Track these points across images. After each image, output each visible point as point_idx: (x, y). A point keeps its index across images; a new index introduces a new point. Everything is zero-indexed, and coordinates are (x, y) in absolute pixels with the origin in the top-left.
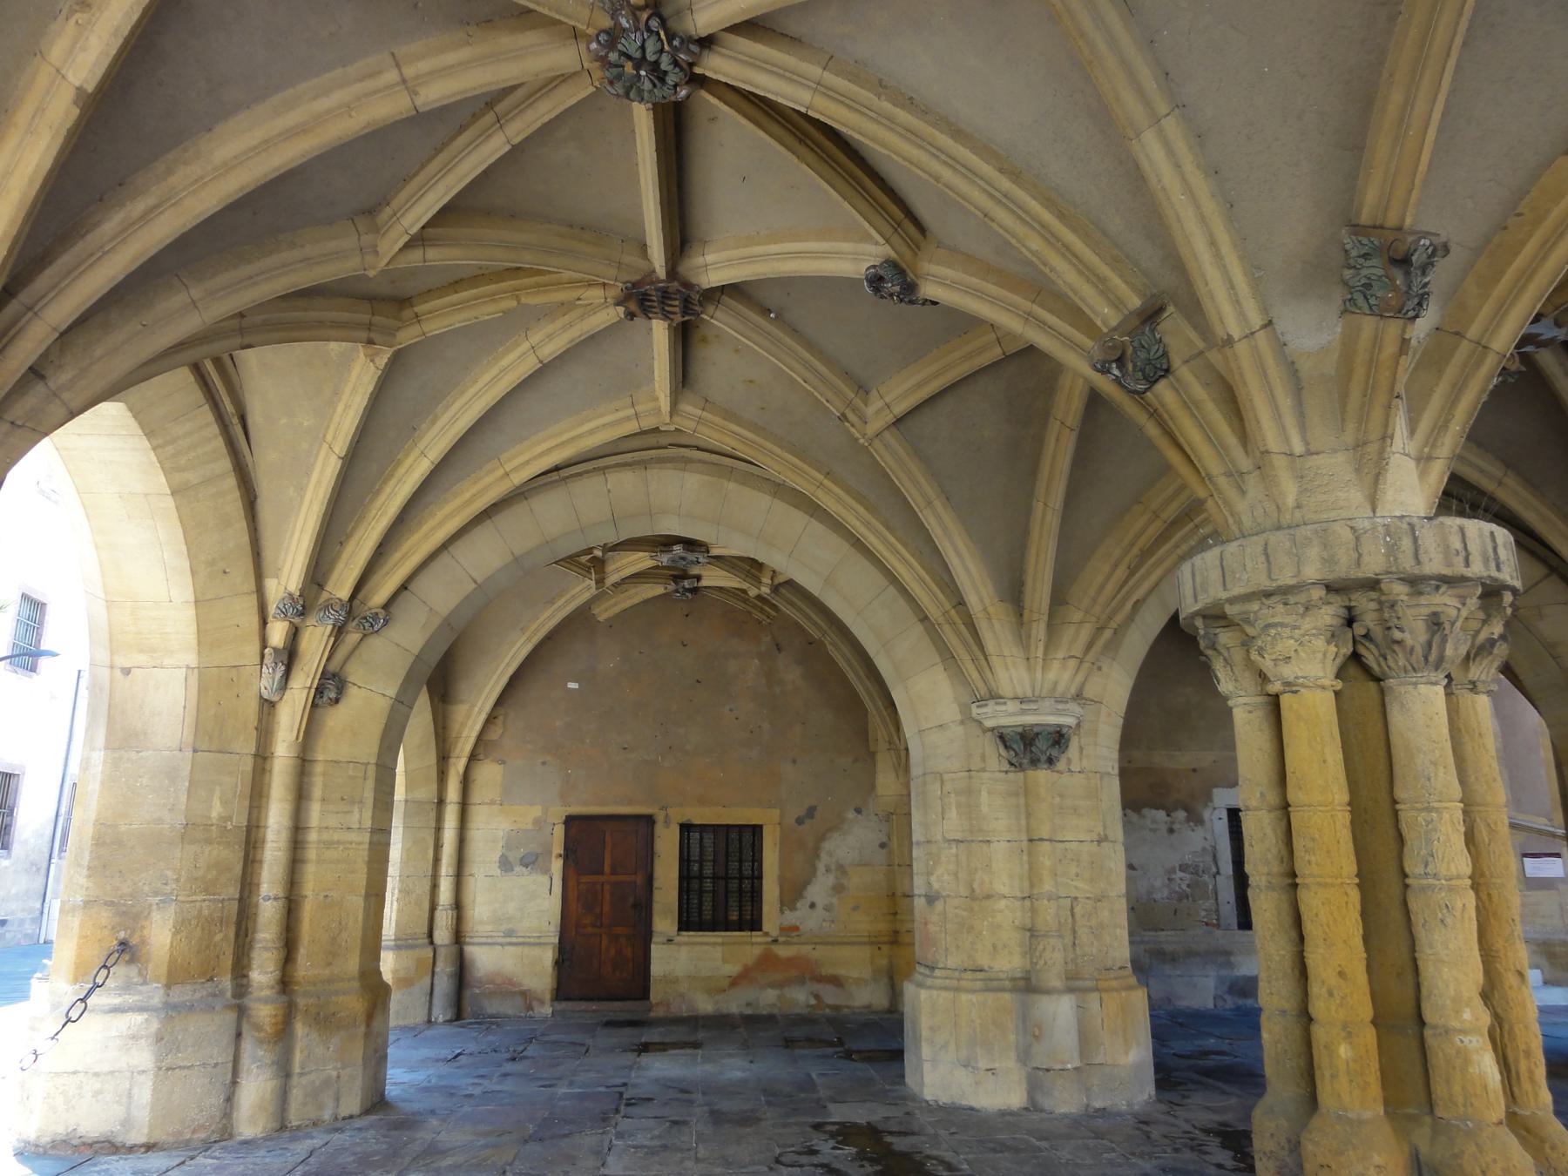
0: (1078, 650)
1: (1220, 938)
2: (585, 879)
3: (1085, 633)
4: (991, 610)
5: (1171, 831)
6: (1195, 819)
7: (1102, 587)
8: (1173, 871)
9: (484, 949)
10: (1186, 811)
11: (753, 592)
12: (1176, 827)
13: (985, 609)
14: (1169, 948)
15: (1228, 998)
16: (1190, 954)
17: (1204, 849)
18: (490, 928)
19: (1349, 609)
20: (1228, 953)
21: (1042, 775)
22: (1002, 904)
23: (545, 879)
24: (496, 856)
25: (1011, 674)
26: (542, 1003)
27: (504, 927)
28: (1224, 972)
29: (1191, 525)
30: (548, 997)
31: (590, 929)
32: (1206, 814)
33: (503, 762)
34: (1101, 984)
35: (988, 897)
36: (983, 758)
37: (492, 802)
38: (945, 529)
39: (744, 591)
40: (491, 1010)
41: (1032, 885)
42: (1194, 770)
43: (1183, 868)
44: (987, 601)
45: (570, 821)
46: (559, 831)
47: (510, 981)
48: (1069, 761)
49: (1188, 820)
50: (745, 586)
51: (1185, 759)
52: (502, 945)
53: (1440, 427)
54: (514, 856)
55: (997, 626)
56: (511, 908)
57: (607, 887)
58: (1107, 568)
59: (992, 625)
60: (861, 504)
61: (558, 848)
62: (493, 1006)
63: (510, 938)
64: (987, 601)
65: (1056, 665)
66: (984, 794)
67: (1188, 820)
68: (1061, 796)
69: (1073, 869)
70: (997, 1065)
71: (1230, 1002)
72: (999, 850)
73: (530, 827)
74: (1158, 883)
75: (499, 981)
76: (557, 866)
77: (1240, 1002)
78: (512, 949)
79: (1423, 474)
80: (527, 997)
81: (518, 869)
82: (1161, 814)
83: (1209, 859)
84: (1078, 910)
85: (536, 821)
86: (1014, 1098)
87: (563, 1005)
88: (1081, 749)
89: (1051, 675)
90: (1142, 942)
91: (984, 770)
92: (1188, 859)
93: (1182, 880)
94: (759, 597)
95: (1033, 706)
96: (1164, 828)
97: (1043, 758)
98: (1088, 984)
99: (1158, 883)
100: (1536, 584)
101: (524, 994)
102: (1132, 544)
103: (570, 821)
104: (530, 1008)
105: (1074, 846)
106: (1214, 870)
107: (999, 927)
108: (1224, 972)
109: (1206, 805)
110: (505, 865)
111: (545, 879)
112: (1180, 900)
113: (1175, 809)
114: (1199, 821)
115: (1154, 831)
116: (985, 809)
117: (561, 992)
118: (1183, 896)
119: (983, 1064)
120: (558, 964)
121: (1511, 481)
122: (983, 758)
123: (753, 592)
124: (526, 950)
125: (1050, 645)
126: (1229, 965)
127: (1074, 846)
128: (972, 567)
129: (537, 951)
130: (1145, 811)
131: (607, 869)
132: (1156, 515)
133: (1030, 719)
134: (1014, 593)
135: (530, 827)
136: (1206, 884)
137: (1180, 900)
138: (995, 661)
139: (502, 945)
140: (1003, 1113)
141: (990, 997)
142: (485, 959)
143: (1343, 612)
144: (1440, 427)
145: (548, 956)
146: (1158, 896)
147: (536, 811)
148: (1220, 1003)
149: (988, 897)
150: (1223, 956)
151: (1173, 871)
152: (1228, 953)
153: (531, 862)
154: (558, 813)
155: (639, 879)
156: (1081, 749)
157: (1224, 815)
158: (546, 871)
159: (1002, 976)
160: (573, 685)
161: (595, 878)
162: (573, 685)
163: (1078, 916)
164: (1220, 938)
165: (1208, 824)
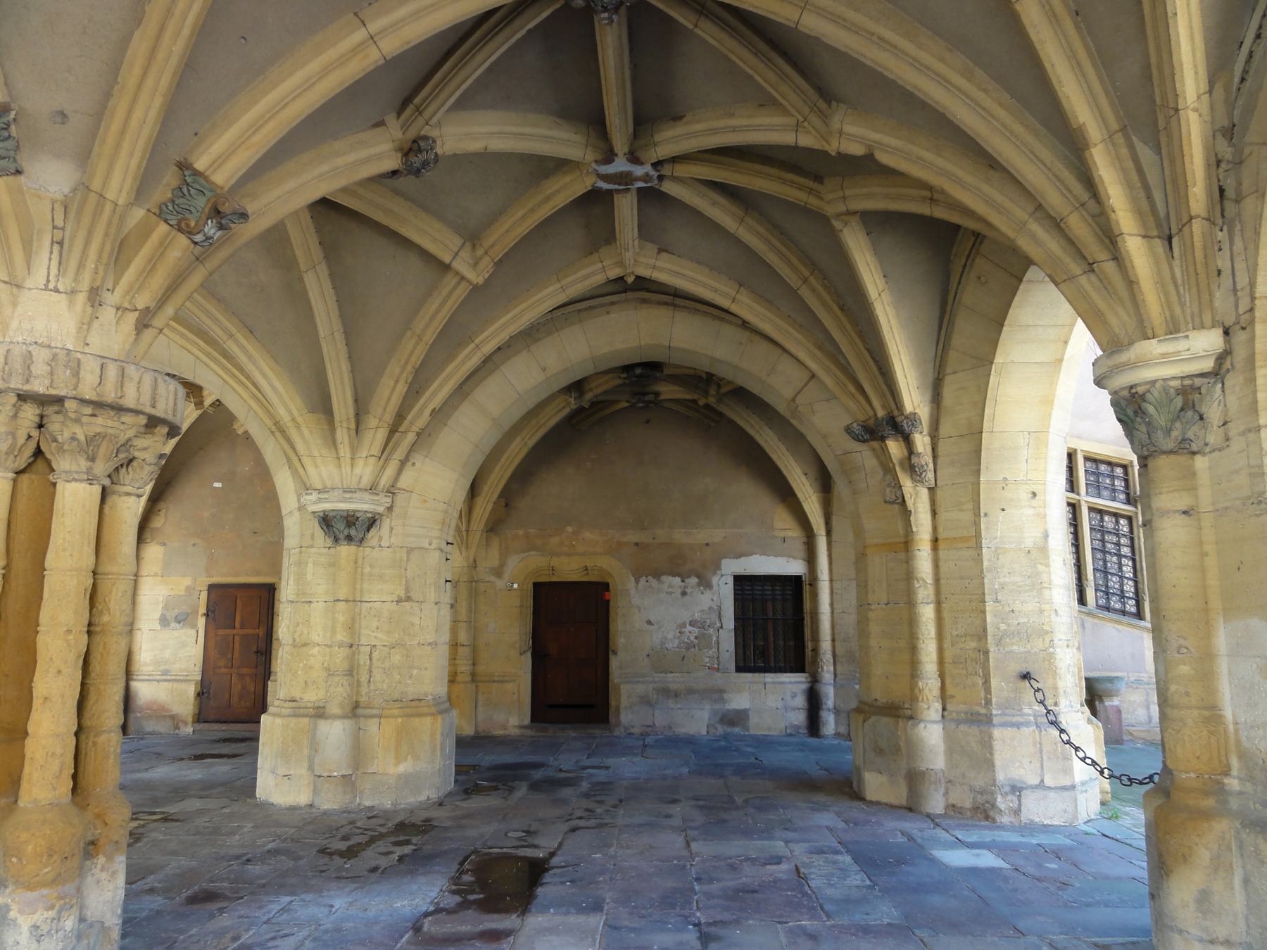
0: (376, 450)
1: (718, 679)
2: (221, 632)
3: (381, 435)
4: (300, 420)
5: (684, 594)
6: (705, 584)
7: (389, 399)
8: (684, 625)
9: (146, 684)
10: (698, 577)
11: (701, 403)
12: (688, 591)
13: (293, 419)
14: (673, 687)
15: (719, 727)
16: (691, 691)
17: (710, 608)
18: (151, 668)
19: (42, 417)
20: (722, 691)
21: (345, 550)
22: (317, 649)
23: (193, 632)
24: (157, 615)
25: (322, 469)
26: (186, 724)
27: (163, 668)
28: (717, 707)
29: (472, 345)
30: (190, 720)
31: (223, 670)
32: (715, 580)
33: (164, 544)
34: (386, 712)
35: (306, 645)
36: (312, 537)
37: (156, 575)
38: (250, 357)
39: (695, 401)
40: (149, 729)
41: (353, 634)
42: (707, 545)
43: (692, 623)
44: (296, 413)
45: (212, 588)
46: (204, 595)
47: (162, 708)
48: (381, 538)
49: (699, 584)
50: (696, 397)
51: (700, 535)
52: (158, 681)
53: (81, 266)
54: (171, 614)
55: (306, 432)
56: (167, 654)
57: (237, 638)
58: (392, 383)
59: (301, 434)
60: (201, 338)
61: (203, 610)
62: (150, 726)
63: (166, 676)
64: (296, 413)
65: (360, 463)
66: (310, 565)
67: (699, 584)
68: (371, 566)
69: (375, 624)
70: (292, 772)
71: (721, 730)
72: (318, 607)
73: (182, 593)
74: (670, 636)
75: (155, 707)
76: (201, 622)
77: (729, 730)
78: (166, 684)
79: (71, 303)
80: (175, 720)
81: (173, 624)
82: (678, 579)
83: (714, 617)
84: (375, 655)
85: (188, 589)
86: (303, 798)
87: (200, 726)
88: (392, 529)
89: (358, 470)
90: (654, 682)
91: (312, 546)
92: (697, 616)
93: (691, 632)
94: (707, 406)
95: (326, 496)
96: (679, 591)
97: (342, 536)
98: (375, 712)
99: (670, 636)
100: (806, 385)
101: (173, 717)
102: (406, 363)
103: (212, 588)
104: (177, 728)
105: (377, 605)
106: (718, 625)
107: (311, 667)
108: (717, 707)
109: (715, 573)
110: (164, 622)
111: (193, 632)
112: (688, 649)
113: (689, 576)
114: (708, 586)
115: (670, 593)
116: (309, 577)
117: (200, 718)
118: (689, 646)
119: (281, 771)
120: (199, 695)
121: (744, 297)
122: (312, 537)
123: (701, 403)
124: (176, 685)
125: (354, 450)
126: (722, 700)
127: (377, 605)
128: (277, 384)
129: (183, 686)
130: (664, 578)
131: (237, 625)
132: (420, 338)
133: (327, 506)
134: (322, 406)
135: (182, 593)
136: (710, 636)
137: (688, 649)
138: (306, 460)
139: (158, 681)
140: (292, 809)
141: (294, 720)
142: (145, 691)
143: (37, 419)
144: (81, 266)
145: (191, 690)
146: (669, 646)
147: (187, 581)
148: (712, 731)
149: (306, 645)
150: (718, 694)
151: (684, 625)
152: (722, 691)
153: (183, 619)
154: (204, 582)
155: (261, 632)
156: (392, 529)
157: (731, 581)
158: (194, 626)
159: (309, 705)
160: (217, 485)
161: (229, 632)
162: (217, 485)
163: (374, 660)
164: (718, 679)
165: (715, 588)
